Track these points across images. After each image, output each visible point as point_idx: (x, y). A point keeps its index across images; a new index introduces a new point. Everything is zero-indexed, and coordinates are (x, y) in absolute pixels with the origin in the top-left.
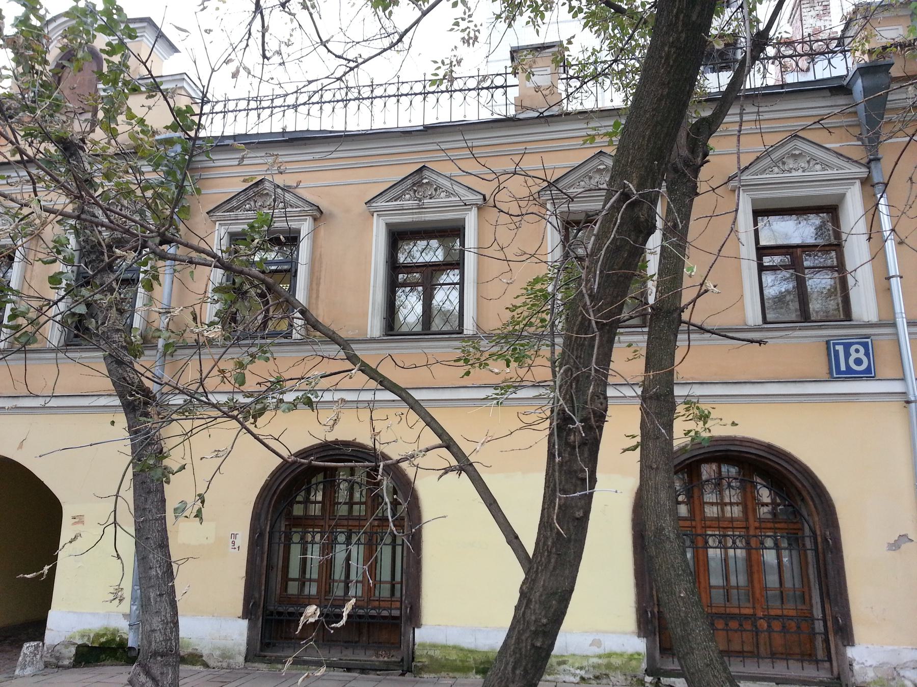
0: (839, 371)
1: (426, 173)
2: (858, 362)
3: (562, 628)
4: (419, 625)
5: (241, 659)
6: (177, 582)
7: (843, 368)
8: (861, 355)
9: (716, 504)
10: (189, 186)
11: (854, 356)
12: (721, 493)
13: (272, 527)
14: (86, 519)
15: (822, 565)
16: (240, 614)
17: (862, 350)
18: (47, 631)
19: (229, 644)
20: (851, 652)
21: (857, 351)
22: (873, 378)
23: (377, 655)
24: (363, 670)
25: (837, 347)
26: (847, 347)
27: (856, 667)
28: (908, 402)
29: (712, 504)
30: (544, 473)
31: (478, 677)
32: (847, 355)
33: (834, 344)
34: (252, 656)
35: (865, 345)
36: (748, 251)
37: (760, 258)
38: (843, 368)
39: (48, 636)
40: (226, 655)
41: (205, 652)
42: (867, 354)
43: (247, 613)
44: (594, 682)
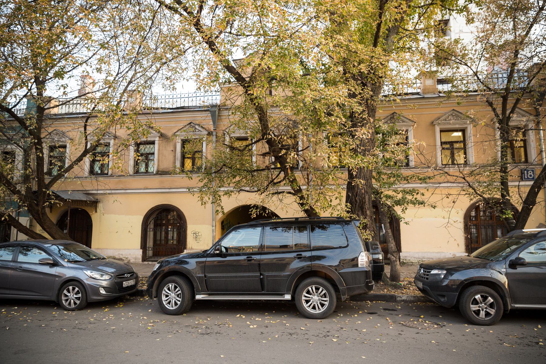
0: (525, 178)
1: (395, 114)
2: (531, 176)
4: (401, 252)
6: (376, 114)
7: (526, 177)
8: (531, 174)
11: (529, 174)
15: (275, 250)
21: (530, 172)
26: (528, 171)
31: (347, 94)
32: (527, 174)
35: (533, 171)
36: (438, 143)
37: (441, 145)
38: (526, 177)
42: (533, 174)
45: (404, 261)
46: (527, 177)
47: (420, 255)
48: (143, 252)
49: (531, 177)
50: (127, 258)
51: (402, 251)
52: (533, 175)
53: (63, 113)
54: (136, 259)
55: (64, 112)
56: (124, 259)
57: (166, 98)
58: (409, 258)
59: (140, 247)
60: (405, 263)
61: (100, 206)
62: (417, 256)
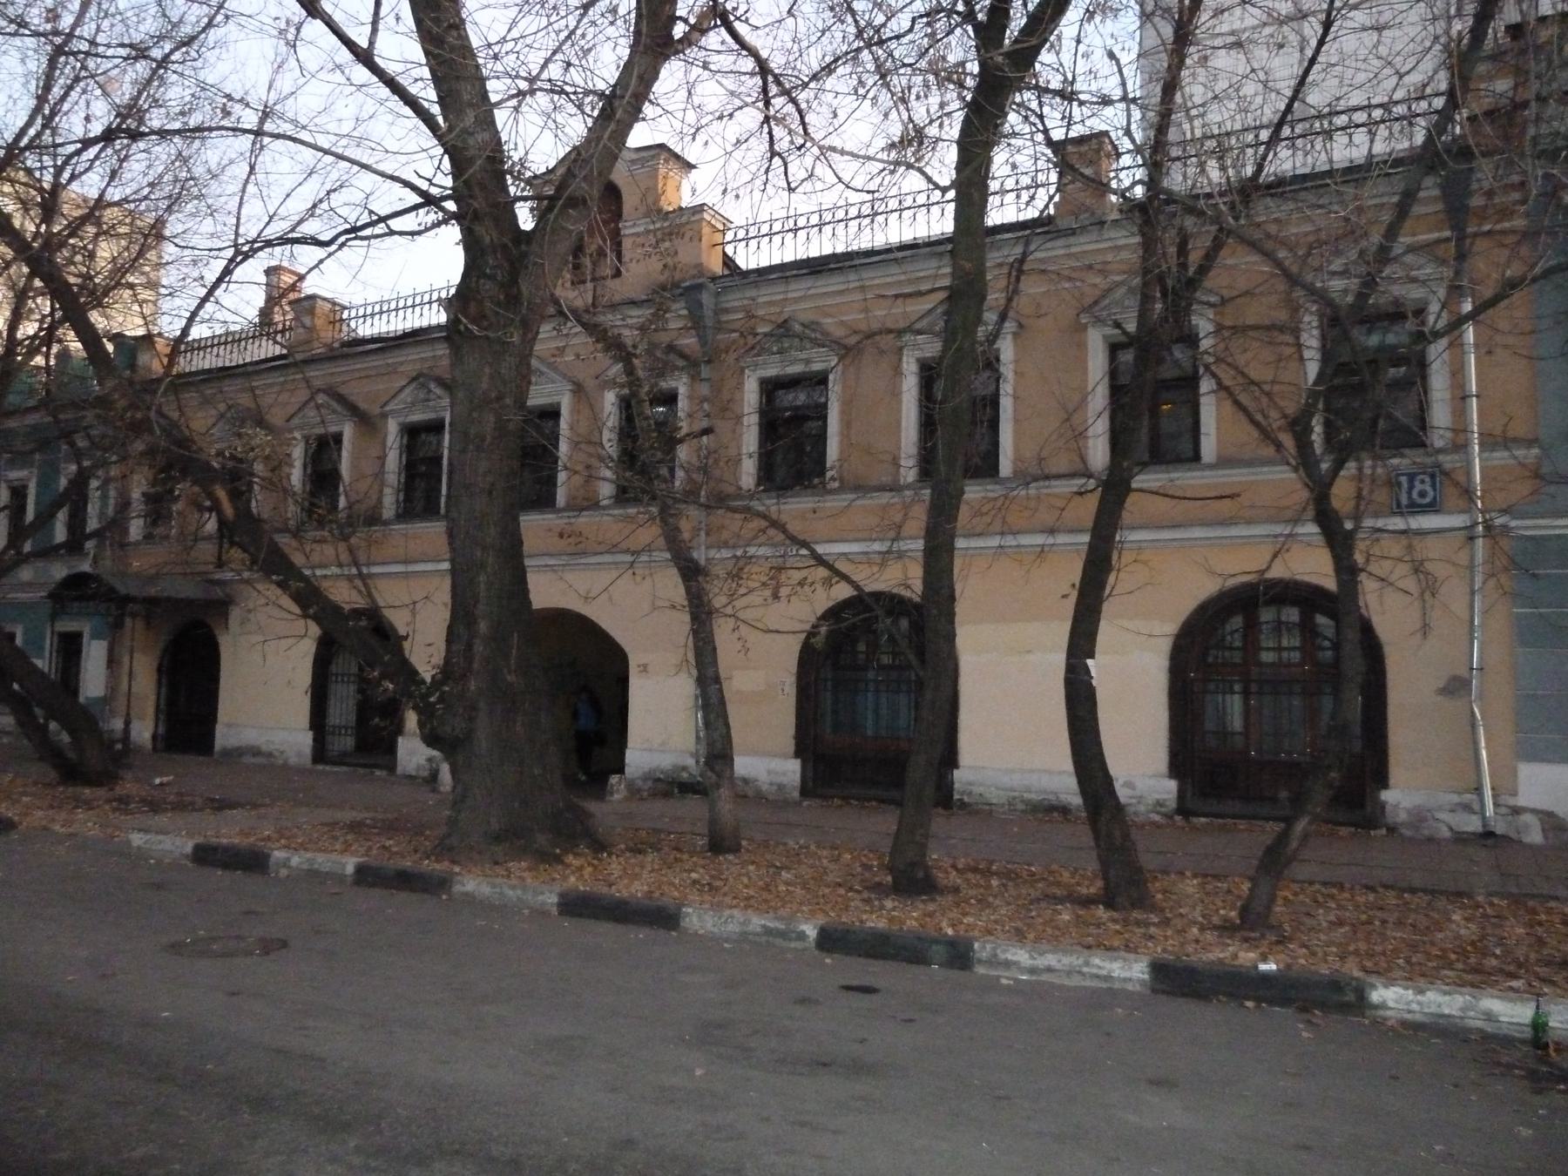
2: (1422, 494)
4: (957, 767)
5: (796, 794)
8: (1428, 488)
9: (1273, 649)
11: (1418, 486)
12: (1280, 636)
14: (650, 668)
17: (1427, 479)
18: (1202, 437)
19: (784, 780)
20: (1386, 796)
21: (1423, 482)
22: (1437, 512)
24: (883, 801)
26: (1412, 478)
27: (1388, 809)
29: (1268, 649)
30: (1066, 627)
32: (1411, 487)
34: (805, 791)
38: (1404, 501)
39: (627, 770)
41: (765, 788)
42: (1433, 486)
43: (799, 753)
45: (966, 799)
46: (1410, 497)
47: (1016, 780)
48: (315, 740)
49: (1427, 500)
50: (282, 752)
51: (1392, 781)
52: (1431, 493)
53: (786, 260)
54: (299, 754)
55: (894, 239)
56: (276, 754)
57: (750, 235)
58: (981, 790)
59: (789, 744)
60: (969, 805)
61: (235, 614)
62: (1006, 780)
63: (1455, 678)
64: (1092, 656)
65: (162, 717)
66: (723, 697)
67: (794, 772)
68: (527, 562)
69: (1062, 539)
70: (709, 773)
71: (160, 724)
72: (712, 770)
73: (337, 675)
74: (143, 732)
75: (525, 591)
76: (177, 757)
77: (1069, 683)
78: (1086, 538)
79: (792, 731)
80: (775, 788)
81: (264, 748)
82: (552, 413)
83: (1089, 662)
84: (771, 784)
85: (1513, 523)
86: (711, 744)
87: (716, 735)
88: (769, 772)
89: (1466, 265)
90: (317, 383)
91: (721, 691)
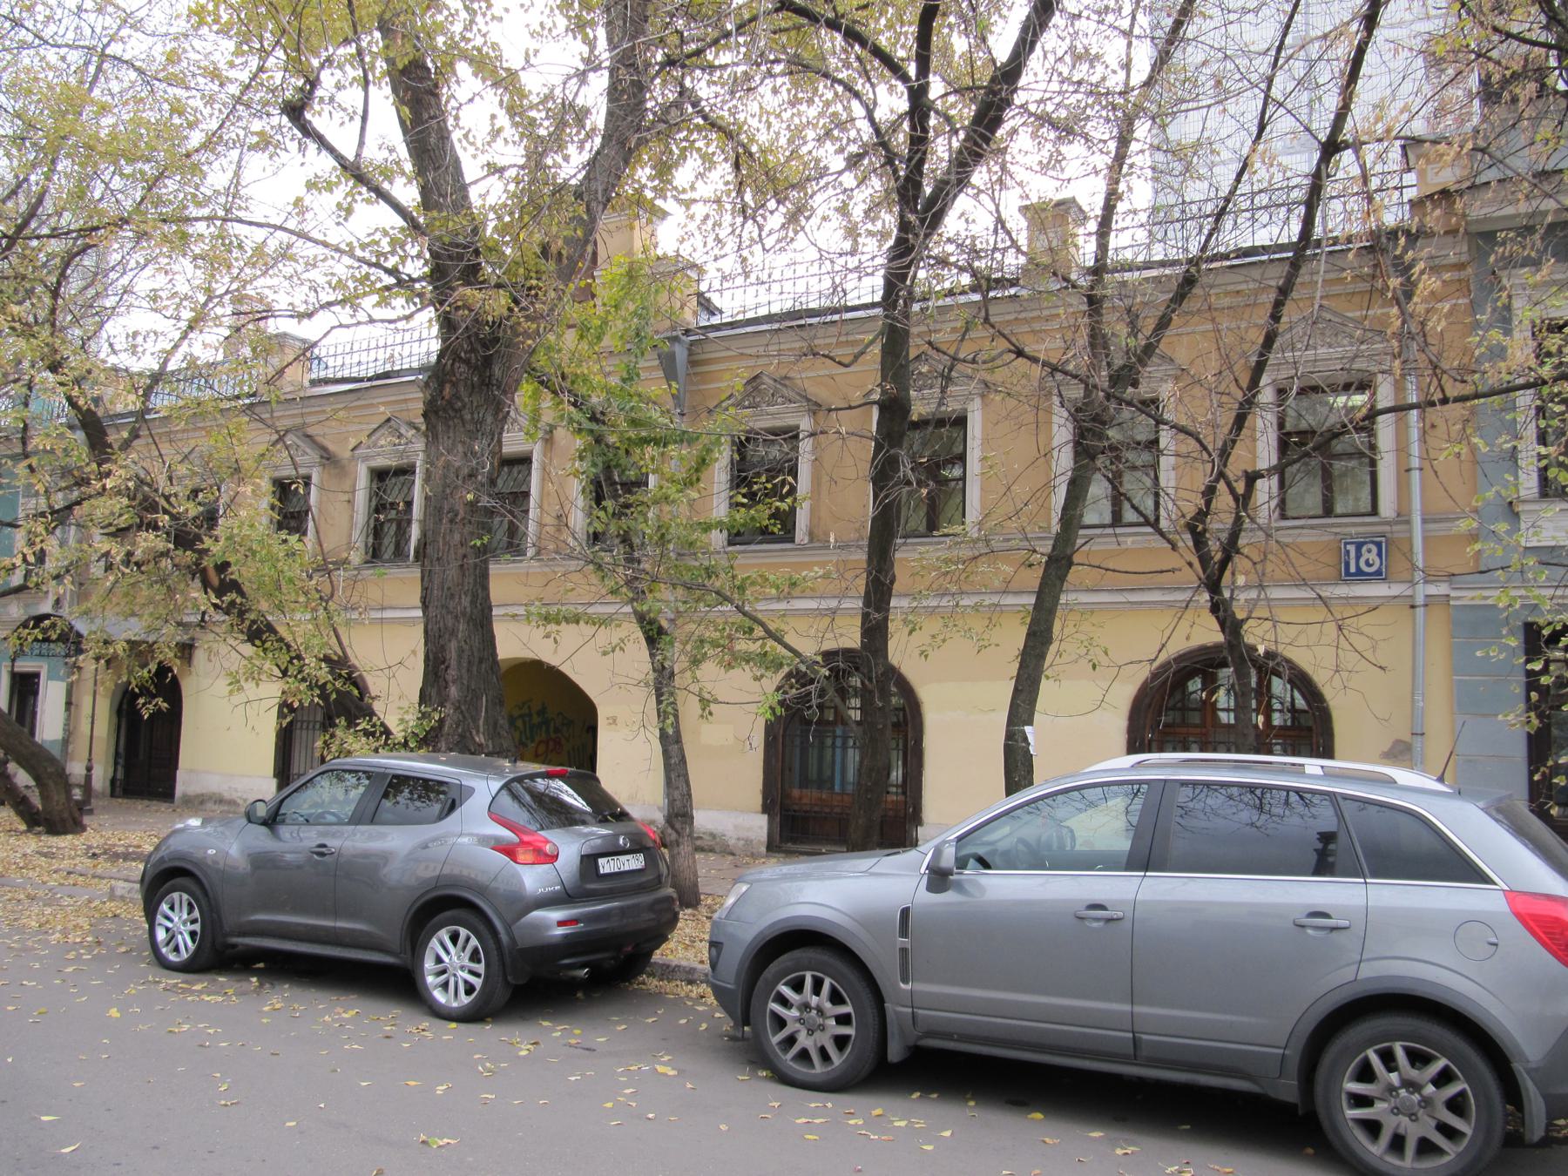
0: (1348, 573)
3: (1039, 706)
7: (1353, 569)
10: (736, 457)
11: (1365, 556)
13: (785, 731)
16: (760, 808)
17: (1374, 549)
19: (752, 835)
23: (321, 851)
25: (1349, 547)
26: (1359, 546)
28: (1413, 607)
32: (1358, 557)
33: (1346, 544)
35: (1379, 545)
38: (1353, 569)
40: (748, 842)
41: (732, 842)
42: (1379, 554)
43: (766, 809)
44: (766, 522)
56: (239, 801)
59: (758, 800)
63: (1398, 742)
64: (1030, 723)
65: (121, 761)
66: (683, 757)
67: (761, 828)
68: (419, 613)
69: (1009, 600)
70: (670, 831)
71: (120, 768)
72: (673, 827)
73: (302, 722)
74: (101, 777)
75: (489, 641)
76: (140, 804)
77: (1009, 751)
78: (1032, 600)
79: (761, 787)
80: (742, 842)
81: (227, 795)
82: (524, 461)
83: (1028, 729)
84: (738, 839)
85: (1453, 594)
86: (671, 802)
87: (677, 794)
88: (736, 827)
89: (1452, 189)
90: (282, 424)
91: (682, 750)
